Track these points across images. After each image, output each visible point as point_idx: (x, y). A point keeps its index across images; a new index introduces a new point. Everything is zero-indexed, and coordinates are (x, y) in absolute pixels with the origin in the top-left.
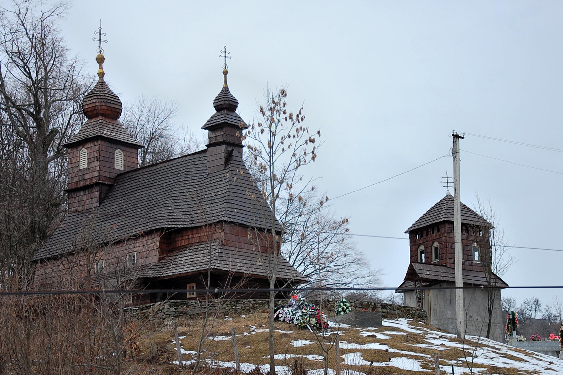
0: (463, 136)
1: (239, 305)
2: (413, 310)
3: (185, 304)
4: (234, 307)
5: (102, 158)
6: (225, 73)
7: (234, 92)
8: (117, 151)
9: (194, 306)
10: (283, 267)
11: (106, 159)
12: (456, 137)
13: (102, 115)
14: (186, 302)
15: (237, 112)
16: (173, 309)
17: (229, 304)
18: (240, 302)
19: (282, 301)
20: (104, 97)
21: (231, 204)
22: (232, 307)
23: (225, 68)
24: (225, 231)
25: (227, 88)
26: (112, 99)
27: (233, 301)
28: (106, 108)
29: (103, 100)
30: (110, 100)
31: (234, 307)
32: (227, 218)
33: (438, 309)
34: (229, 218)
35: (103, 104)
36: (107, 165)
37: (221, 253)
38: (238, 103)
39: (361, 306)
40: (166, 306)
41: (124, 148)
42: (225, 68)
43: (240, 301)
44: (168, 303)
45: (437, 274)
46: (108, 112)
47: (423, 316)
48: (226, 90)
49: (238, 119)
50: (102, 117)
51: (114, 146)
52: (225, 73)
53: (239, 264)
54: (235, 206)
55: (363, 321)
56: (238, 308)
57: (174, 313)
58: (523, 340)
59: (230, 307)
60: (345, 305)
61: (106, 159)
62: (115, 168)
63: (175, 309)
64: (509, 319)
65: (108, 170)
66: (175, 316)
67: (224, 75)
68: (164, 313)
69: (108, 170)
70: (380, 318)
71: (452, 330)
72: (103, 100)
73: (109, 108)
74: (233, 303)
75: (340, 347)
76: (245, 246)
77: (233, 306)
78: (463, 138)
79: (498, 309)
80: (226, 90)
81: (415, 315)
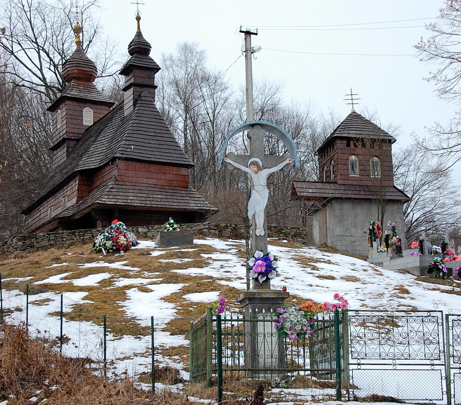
0: (256, 32)
1: (88, 234)
2: (287, 229)
3: (33, 238)
4: (81, 238)
5: (70, 116)
6: (138, 19)
7: (147, 37)
8: (85, 109)
9: (42, 238)
10: (188, 198)
11: (73, 117)
12: (248, 33)
13: (75, 78)
14: (33, 235)
15: (150, 55)
16: (21, 243)
17: (78, 235)
18: (89, 232)
19: (133, 228)
20: (75, 62)
21: (128, 141)
22: (80, 237)
23: (138, 14)
24: (118, 168)
25: (141, 33)
26: (83, 63)
27: (82, 232)
28: (76, 71)
29: (74, 65)
30: (81, 64)
31: (81, 238)
32: (119, 154)
33: (331, 228)
34: (122, 154)
35: (74, 68)
36: (75, 122)
37: (112, 188)
38: (151, 47)
39: (216, 228)
40: (14, 241)
41: (93, 106)
42: (138, 14)
43: (88, 231)
44: (17, 237)
45: (322, 191)
46: (81, 76)
47: (301, 235)
48: (139, 34)
49: (150, 61)
50: (74, 80)
51: (83, 105)
52: (138, 19)
53: (131, 198)
54: (133, 143)
55: (170, 241)
56: (86, 237)
57: (21, 246)
58: (383, 250)
59: (78, 238)
60: (172, 227)
61: (73, 117)
62: (84, 124)
63: (24, 243)
64: (370, 230)
65: (76, 126)
66: (21, 249)
67: (137, 21)
68: (13, 247)
69: (76, 126)
70: (190, 236)
71: (342, 247)
72: (74, 65)
73: (79, 71)
74: (81, 233)
75: (264, 271)
76: (143, 180)
77: (82, 236)
78: (256, 34)
79: (400, 222)
80: (139, 34)
81: (290, 234)
